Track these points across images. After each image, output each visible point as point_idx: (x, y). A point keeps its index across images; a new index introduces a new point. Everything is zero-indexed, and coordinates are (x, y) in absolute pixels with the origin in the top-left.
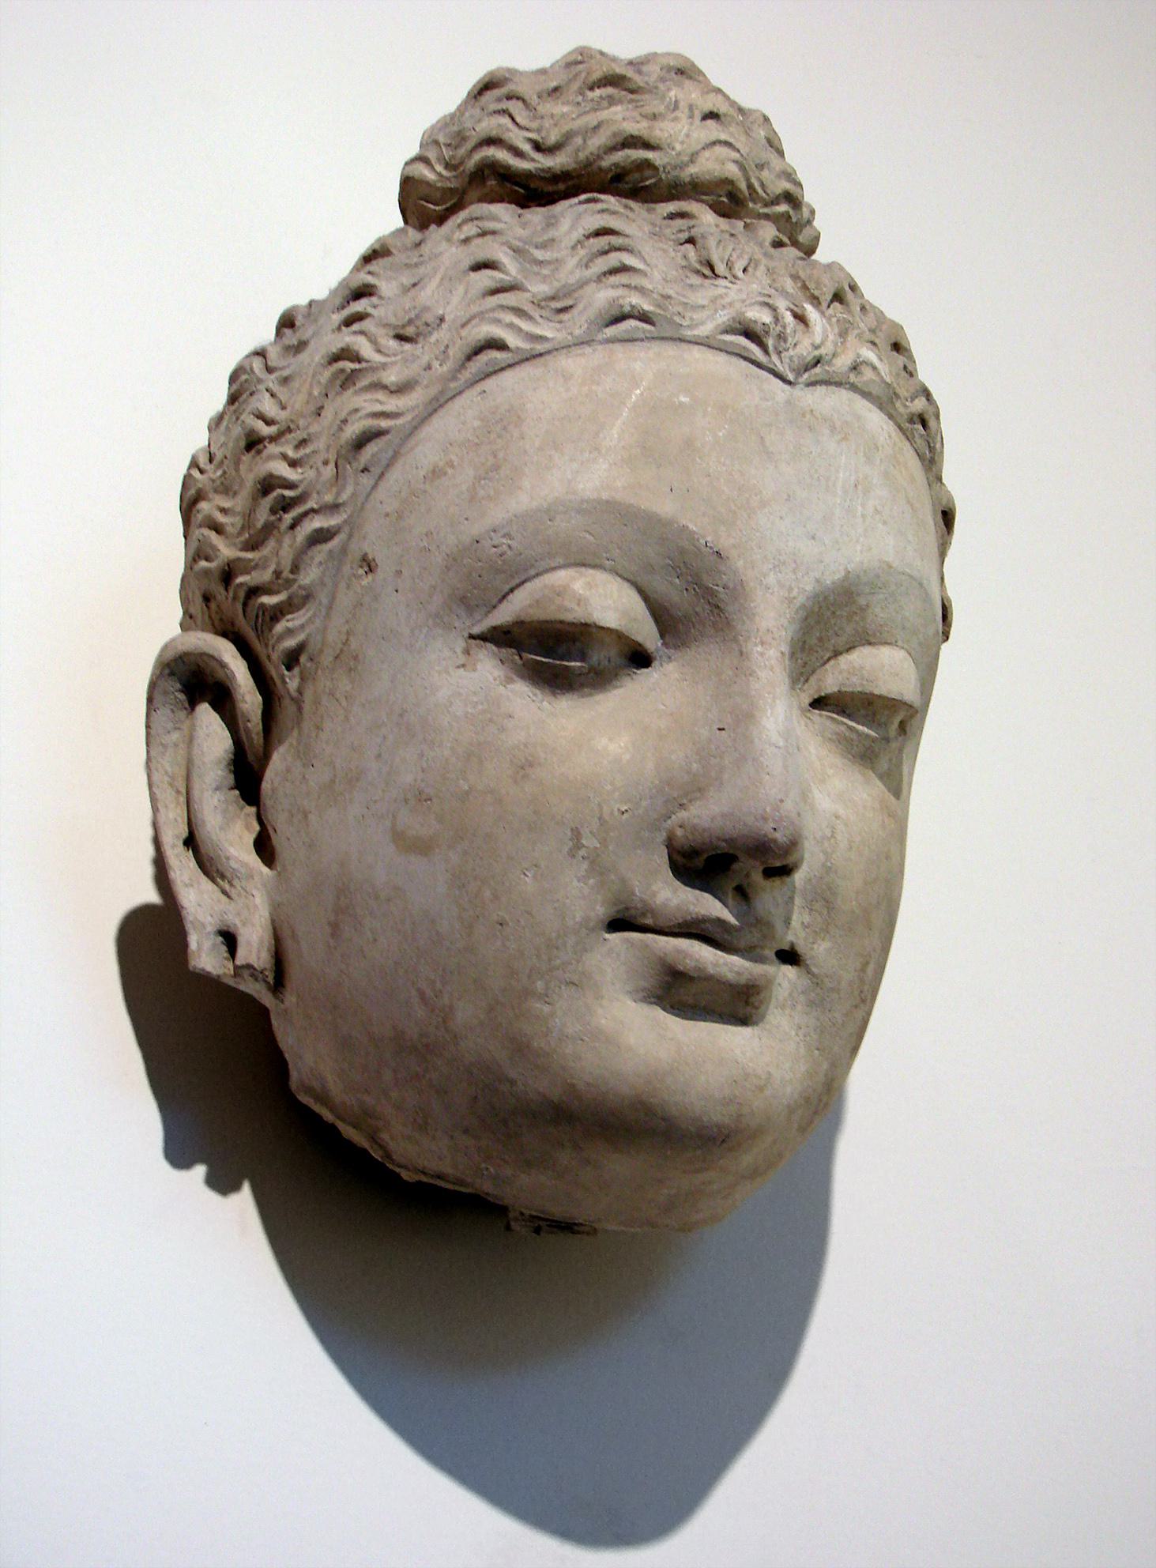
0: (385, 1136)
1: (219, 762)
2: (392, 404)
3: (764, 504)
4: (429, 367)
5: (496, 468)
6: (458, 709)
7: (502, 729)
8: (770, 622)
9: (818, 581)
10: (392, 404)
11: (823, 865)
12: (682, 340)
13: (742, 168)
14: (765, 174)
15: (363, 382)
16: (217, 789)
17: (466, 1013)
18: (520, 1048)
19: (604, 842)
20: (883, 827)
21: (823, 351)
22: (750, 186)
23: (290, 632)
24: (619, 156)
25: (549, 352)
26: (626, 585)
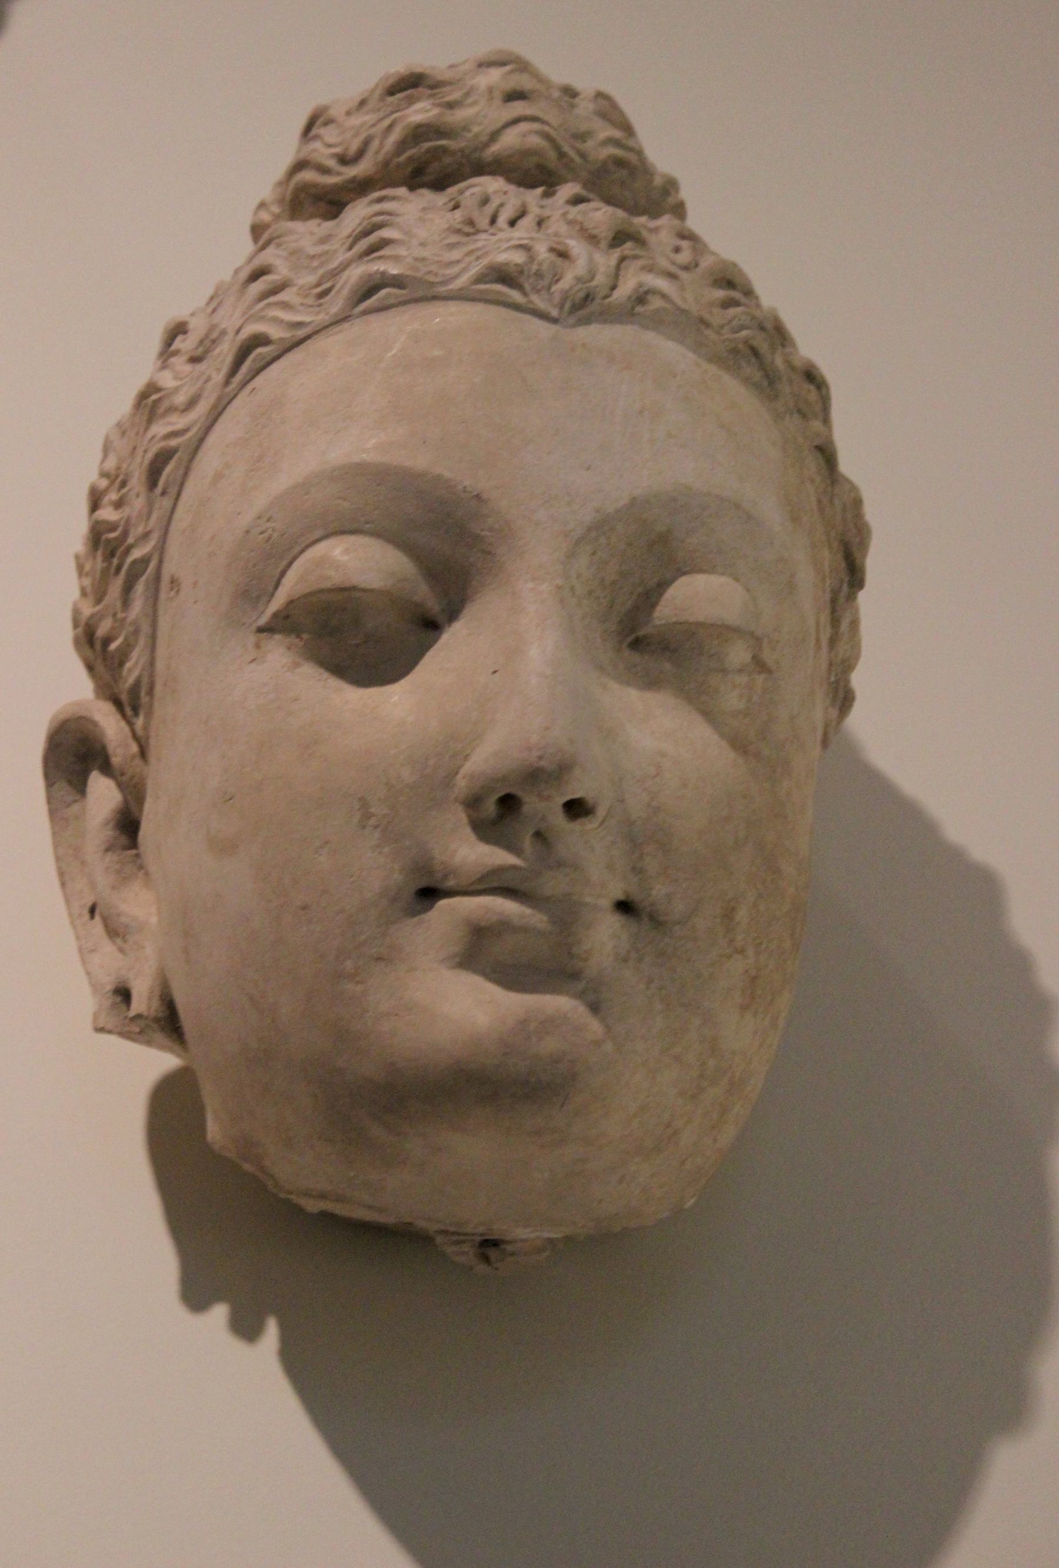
0: (267, 1163)
1: (106, 823)
9: (598, 511)
12: (435, 298)
13: (547, 137)
14: (590, 144)
15: (161, 410)
16: (107, 850)
22: (562, 155)
23: (130, 670)
25: (308, 337)
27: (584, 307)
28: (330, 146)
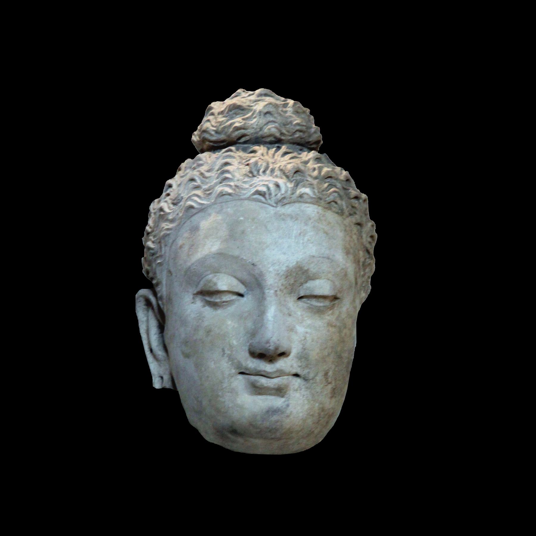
2: (171, 226)
3: (267, 247)
4: (178, 214)
5: (193, 245)
6: (193, 316)
7: (203, 321)
8: (272, 281)
10: (171, 226)
11: (302, 348)
17: (205, 403)
18: (218, 411)
19: (232, 351)
20: (328, 331)
21: (285, 195)
24: (237, 133)
26: (230, 277)
27: (282, 202)
28: (213, 126)
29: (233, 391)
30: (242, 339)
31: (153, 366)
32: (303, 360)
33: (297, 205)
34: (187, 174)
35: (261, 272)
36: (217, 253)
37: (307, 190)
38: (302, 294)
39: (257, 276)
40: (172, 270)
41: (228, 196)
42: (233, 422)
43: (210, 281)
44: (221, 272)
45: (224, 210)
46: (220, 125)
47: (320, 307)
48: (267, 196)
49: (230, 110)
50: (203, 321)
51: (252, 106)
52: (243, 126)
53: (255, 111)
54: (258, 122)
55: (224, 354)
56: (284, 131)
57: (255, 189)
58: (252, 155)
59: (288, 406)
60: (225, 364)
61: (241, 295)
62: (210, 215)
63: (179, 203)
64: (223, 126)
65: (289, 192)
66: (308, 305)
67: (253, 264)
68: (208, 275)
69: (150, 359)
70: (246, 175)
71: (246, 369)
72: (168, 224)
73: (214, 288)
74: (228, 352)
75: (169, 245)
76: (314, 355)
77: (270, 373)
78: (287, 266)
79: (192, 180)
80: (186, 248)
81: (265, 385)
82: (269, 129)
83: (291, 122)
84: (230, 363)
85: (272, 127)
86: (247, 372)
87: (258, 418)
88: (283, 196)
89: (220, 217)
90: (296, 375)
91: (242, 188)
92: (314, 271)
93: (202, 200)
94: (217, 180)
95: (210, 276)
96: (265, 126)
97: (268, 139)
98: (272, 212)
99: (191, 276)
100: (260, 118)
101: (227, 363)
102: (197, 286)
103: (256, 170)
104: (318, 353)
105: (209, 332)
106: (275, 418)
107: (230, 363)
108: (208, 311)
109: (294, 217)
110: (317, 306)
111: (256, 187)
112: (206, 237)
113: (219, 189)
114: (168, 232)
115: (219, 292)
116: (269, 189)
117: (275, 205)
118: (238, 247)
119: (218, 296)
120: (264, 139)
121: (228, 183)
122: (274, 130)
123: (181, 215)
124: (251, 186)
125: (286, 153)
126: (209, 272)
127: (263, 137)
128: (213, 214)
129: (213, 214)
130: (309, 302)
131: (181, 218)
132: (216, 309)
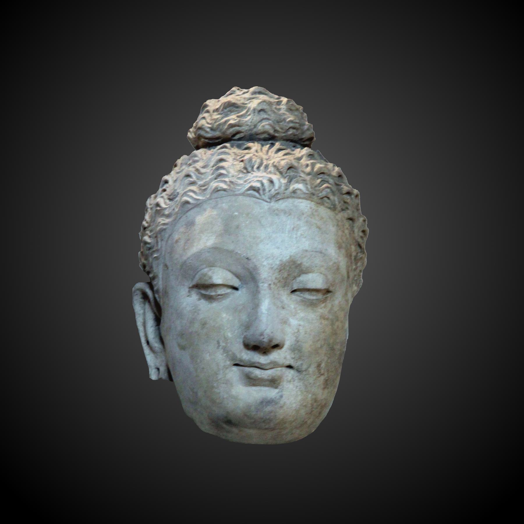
2: (167, 221)
3: (261, 241)
4: (174, 210)
5: (188, 240)
6: (188, 309)
7: (198, 314)
8: (266, 274)
10: (167, 221)
11: (296, 340)
17: (200, 394)
18: (213, 402)
19: (227, 343)
20: (321, 323)
21: (279, 191)
24: (231, 130)
26: (225, 270)
27: (276, 197)
28: (208, 123)
29: (228, 382)
30: (236, 331)
31: (150, 358)
32: (296, 352)
33: (290, 200)
34: (183, 170)
35: (255, 266)
36: (212, 248)
37: (300, 186)
38: (295, 288)
39: (251, 270)
40: (168, 264)
41: (222, 192)
42: (228, 412)
43: (205, 275)
44: (216, 266)
45: (219, 206)
46: (215, 122)
47: (313, 300)
48: (261, 192)
49: (225, 108)
50: (198, 314)
51: (246, 104)
52: (237, 123)
53: (249, 109)
54: (253, 120)
55: (219, 346)
56: (278, 128)
57: (249, 185)
58: (246, 151)
59: (281, 396)
60: (220, 356)
61: (236, 289)
62: (205, 210)
63: (175, 198)
64: (218, 123)
65: (283, 188)
66: (301, 298)
67: (247, 258)
68: (203, 269)
69: (146, 350)
70: (240, 171)
71: (241, 360)
72: (164, 219)
73: (209, 282)
74: (222, 344)
75: (165, 240)
76: (307, 347)
77: (264, 364)
78: (281, 261)
79: (188, 176)
80: (182, 242)
81: (260, 377)
82: (263, 126)
83: (284, 120)
84: (225, 355)
85: (266, 125)
86: (242, 364)
87: (253, 408)
88: (277, 192)
89: (215, 213)
90: (290, 367)
91: (236, 184)
92: (307, 265)
93: (198, 195)
94: (213, 176)
95: (206, 270)
96: (259, 124)
97: (262, 136)
98: (266, 207)
99: (187, 270)
100: (254, 115)
101: (222, 354)
102: (192, 280)
103: (250, 166)
104: (311, 346)
105: (204, 324)
106: (269, 408)
107: (225, 355)
108: (203, 304)
109: (288, 213)
110: (310, 299)
111: (250, 182)
112: (202, 232)
113: (214, 185)
114: (165, 227)
115: (214, 286)
116: (263, 184)
117: (269, 200)
118: (233, 242)
119: (213, 289)
120: (258, 136)
121: (223, 179)
122: (268, 127)
123: (177, 210)
124: (245, 181)
125: (279, 150)
126: (204, 266)
127: (257, 134)
128: (209, 210)
129: (209, 210)
130: (302, 295)
131: (177, 213)
132: (211, 302)
